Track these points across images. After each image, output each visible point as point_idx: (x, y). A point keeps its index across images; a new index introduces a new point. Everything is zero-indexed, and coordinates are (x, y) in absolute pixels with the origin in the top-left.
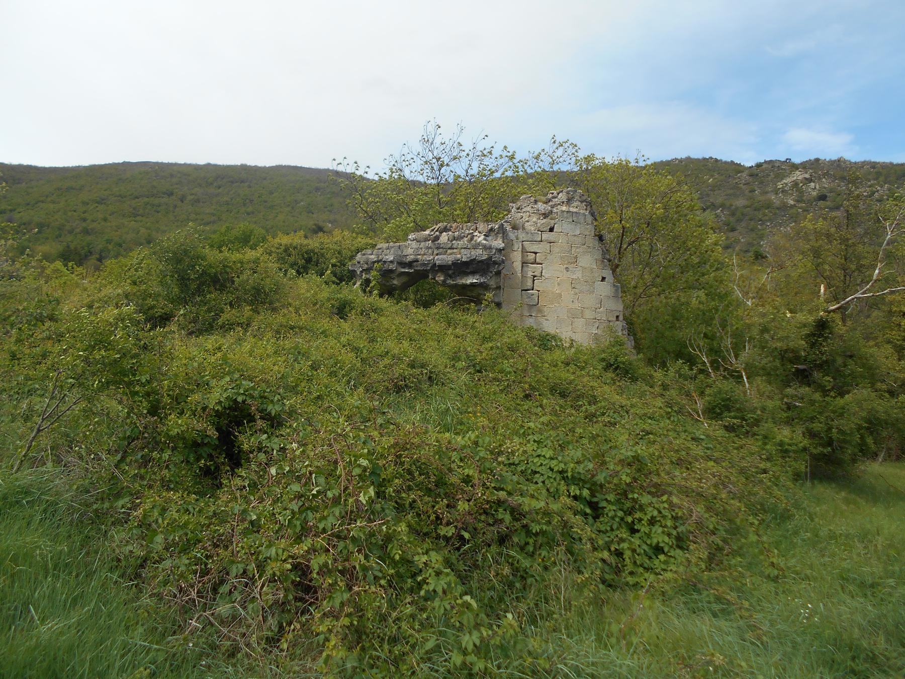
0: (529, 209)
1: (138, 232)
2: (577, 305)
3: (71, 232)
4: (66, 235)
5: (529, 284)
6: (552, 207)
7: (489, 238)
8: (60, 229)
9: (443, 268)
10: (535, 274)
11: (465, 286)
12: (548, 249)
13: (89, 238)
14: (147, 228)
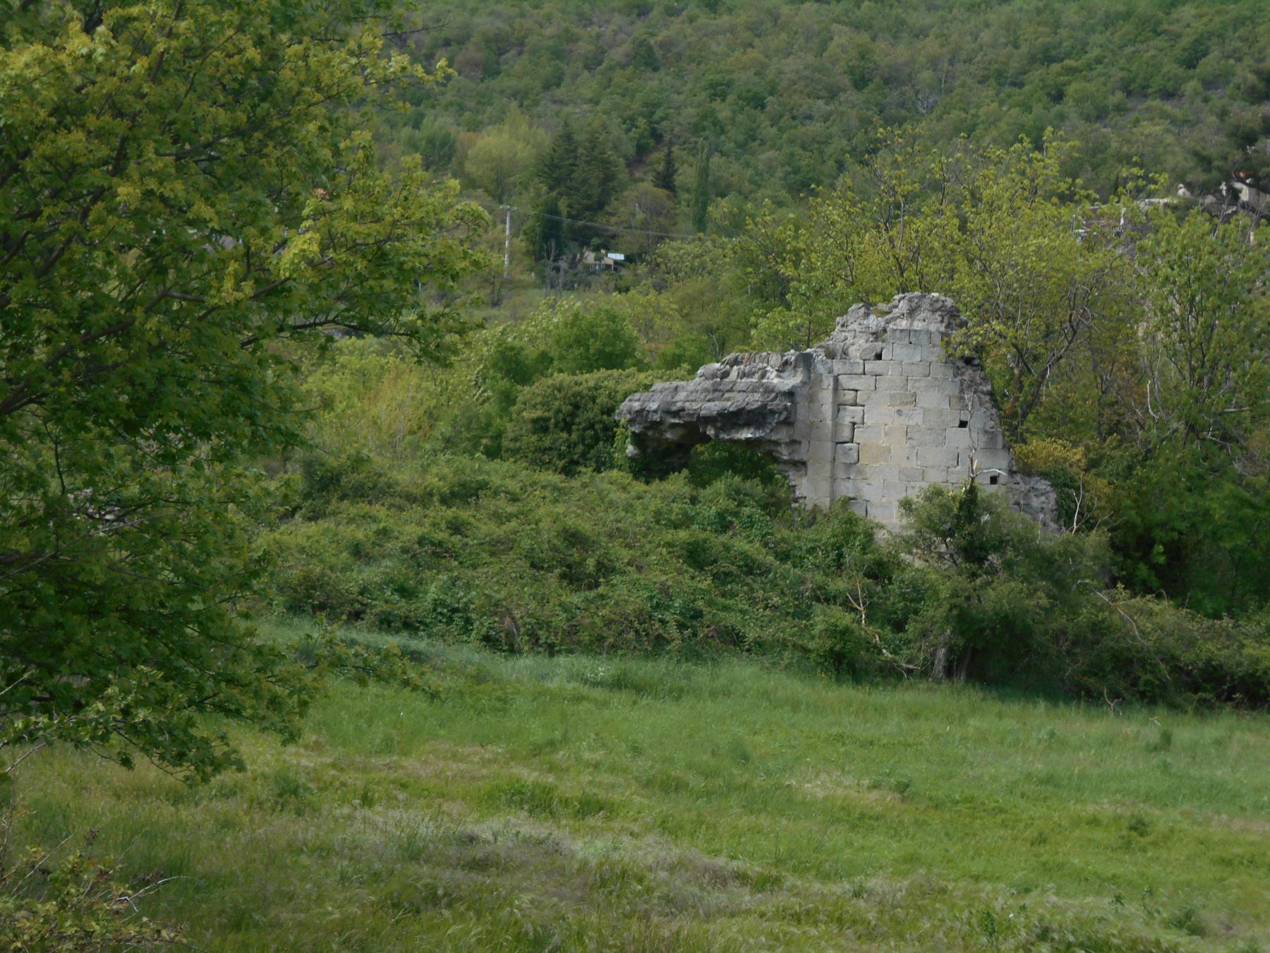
0: (855, 326)
1: (823, 47)
2: (914, 463)
3: (591, 64)
4: (575, 76)
5: (846, 434)
6: (888, 322)
7: (785, 374)
8: (557, 54)
9: (708, 420)
10: (855, 420)
11: (739, 441)
12: (873, 384)
13: (652, 83)
14: (858, 26)
